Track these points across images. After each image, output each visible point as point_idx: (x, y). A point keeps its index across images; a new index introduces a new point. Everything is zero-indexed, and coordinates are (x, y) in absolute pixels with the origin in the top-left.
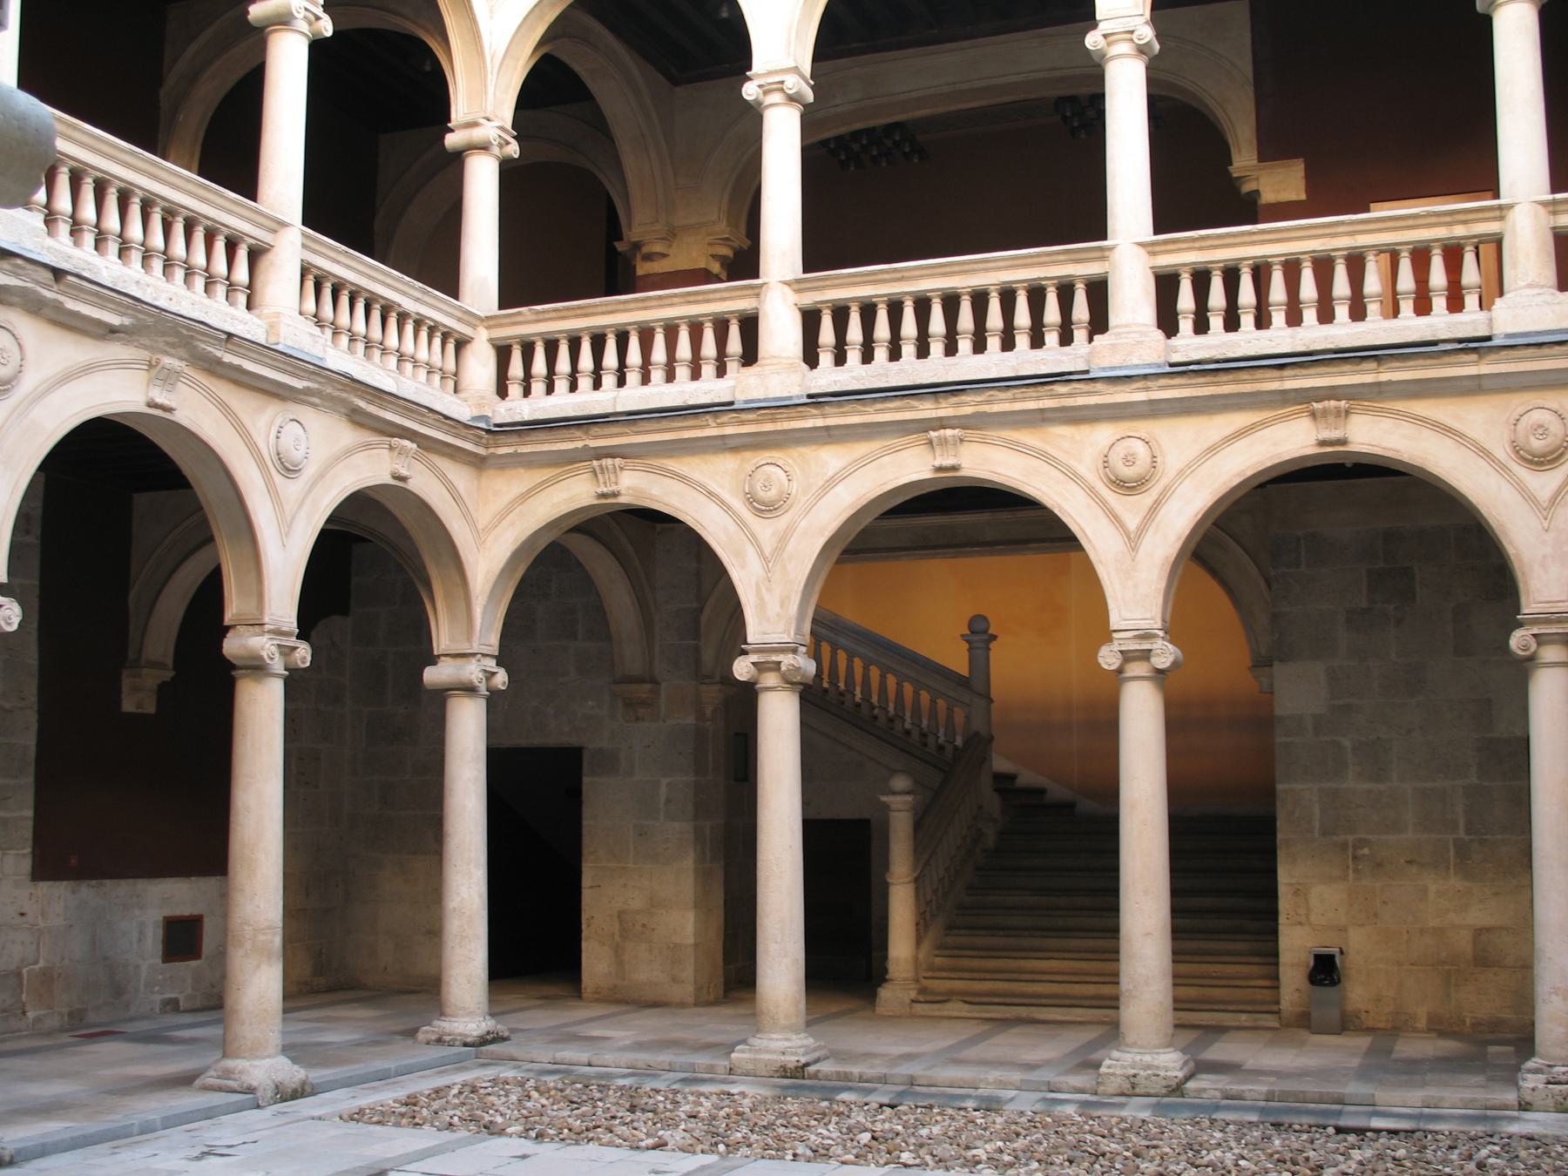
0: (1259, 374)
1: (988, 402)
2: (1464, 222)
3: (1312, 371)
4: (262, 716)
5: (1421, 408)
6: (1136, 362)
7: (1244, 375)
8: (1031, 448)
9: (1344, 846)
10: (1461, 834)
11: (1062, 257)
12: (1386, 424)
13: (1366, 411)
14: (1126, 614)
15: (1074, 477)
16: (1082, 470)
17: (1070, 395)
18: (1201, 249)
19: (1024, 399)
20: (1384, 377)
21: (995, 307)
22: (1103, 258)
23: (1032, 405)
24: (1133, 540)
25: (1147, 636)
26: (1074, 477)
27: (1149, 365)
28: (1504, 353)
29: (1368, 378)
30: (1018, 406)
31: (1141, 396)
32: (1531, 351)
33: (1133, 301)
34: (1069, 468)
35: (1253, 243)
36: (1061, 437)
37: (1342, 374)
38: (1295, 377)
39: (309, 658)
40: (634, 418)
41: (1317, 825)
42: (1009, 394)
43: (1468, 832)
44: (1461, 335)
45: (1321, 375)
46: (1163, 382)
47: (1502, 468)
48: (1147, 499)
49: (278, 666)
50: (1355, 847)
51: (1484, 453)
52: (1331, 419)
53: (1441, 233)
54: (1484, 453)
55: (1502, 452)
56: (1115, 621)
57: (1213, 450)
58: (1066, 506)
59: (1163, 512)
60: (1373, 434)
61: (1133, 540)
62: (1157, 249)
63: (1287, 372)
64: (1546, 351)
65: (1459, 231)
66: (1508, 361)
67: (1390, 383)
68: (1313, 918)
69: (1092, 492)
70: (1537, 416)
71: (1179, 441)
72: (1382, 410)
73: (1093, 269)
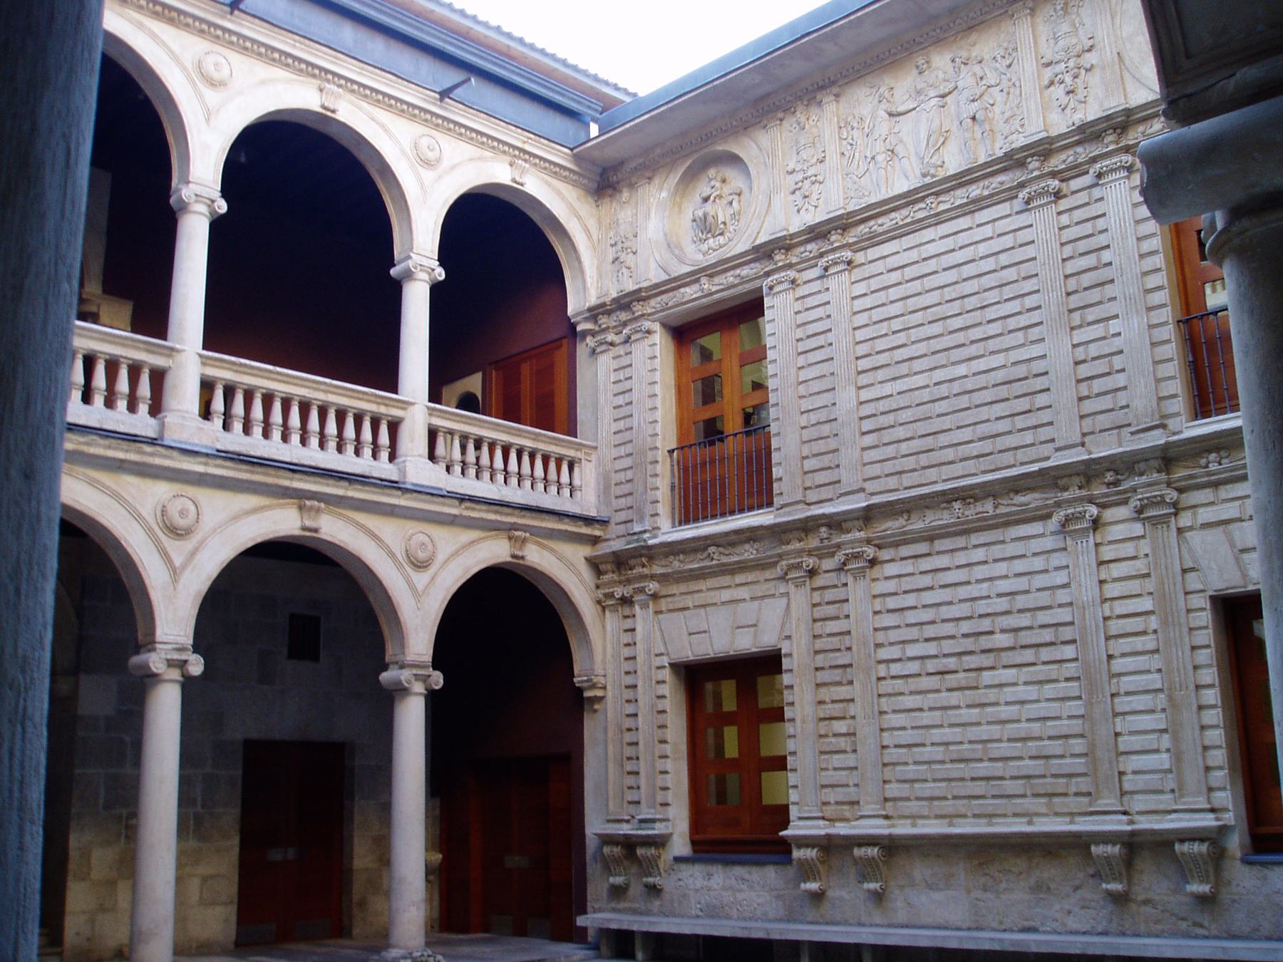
0: (281, 473)
1: (88, 444)
2: (386, 405)
3: (312, 479)
4: (165, 714)
5: (361, 517)
6: (196, 441)
7: (271, 471)
8: (108, 488)
9: (120, 818)
10: (199, 809)
11: (142, 346)
12: (340, 524)
13: (331, 513)
14: (166, 630)
15: (138, 517)
16: (144, 514)
17: (151, 454)
18: (236, 371)
19: (115, 449)
20: (350, 493)
21: (123, 375)
22: (169, 356)
23: (121, 455)
24: (175, 573)
25: (181, 649)
26: (138, 517)
27: (206, 447)
28: (415, 495)
29: (340, 492)
30: (110, 453)
31: (492, 517)
32: (428, 497)
33: (183, 395)
34: (136, 510)
35: (268, 379)
36: (130, 485)
37: (328, 485)
38: (300, 480)
39: (442, 681)
40: (295, 469)
41: (101, 801)
42: (107, 442)
43: (203, 806)
44: (383, 477)
45: (315, 483)
46: (219, 462)
47: (399, 566)
48: (188, 545)
49: (419, 688)
50: (127, 819)
51: (392, 555)
52: (313, 513)
53: (373, 407)
54: (392, 555)
55: (400, 556)
56: (160, 634)
57: (236, 518)
58: (130, 539)
59: (198, 556)
60: (336, 530)
61: (175, 573)
62: (209, 362)
63: (297, 476)
64: (435, 499)
65: (383, 410)
66: (415, 500)
67: (352, 498)
68: (92, 876)
69: (149, 531)
70: (423, 538)
71: (216, 505)
72: (340, 514)
73: (159, 361)
